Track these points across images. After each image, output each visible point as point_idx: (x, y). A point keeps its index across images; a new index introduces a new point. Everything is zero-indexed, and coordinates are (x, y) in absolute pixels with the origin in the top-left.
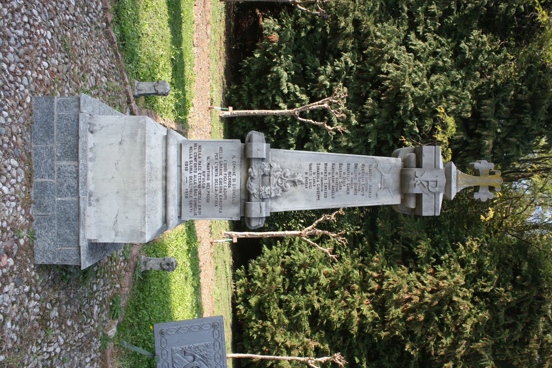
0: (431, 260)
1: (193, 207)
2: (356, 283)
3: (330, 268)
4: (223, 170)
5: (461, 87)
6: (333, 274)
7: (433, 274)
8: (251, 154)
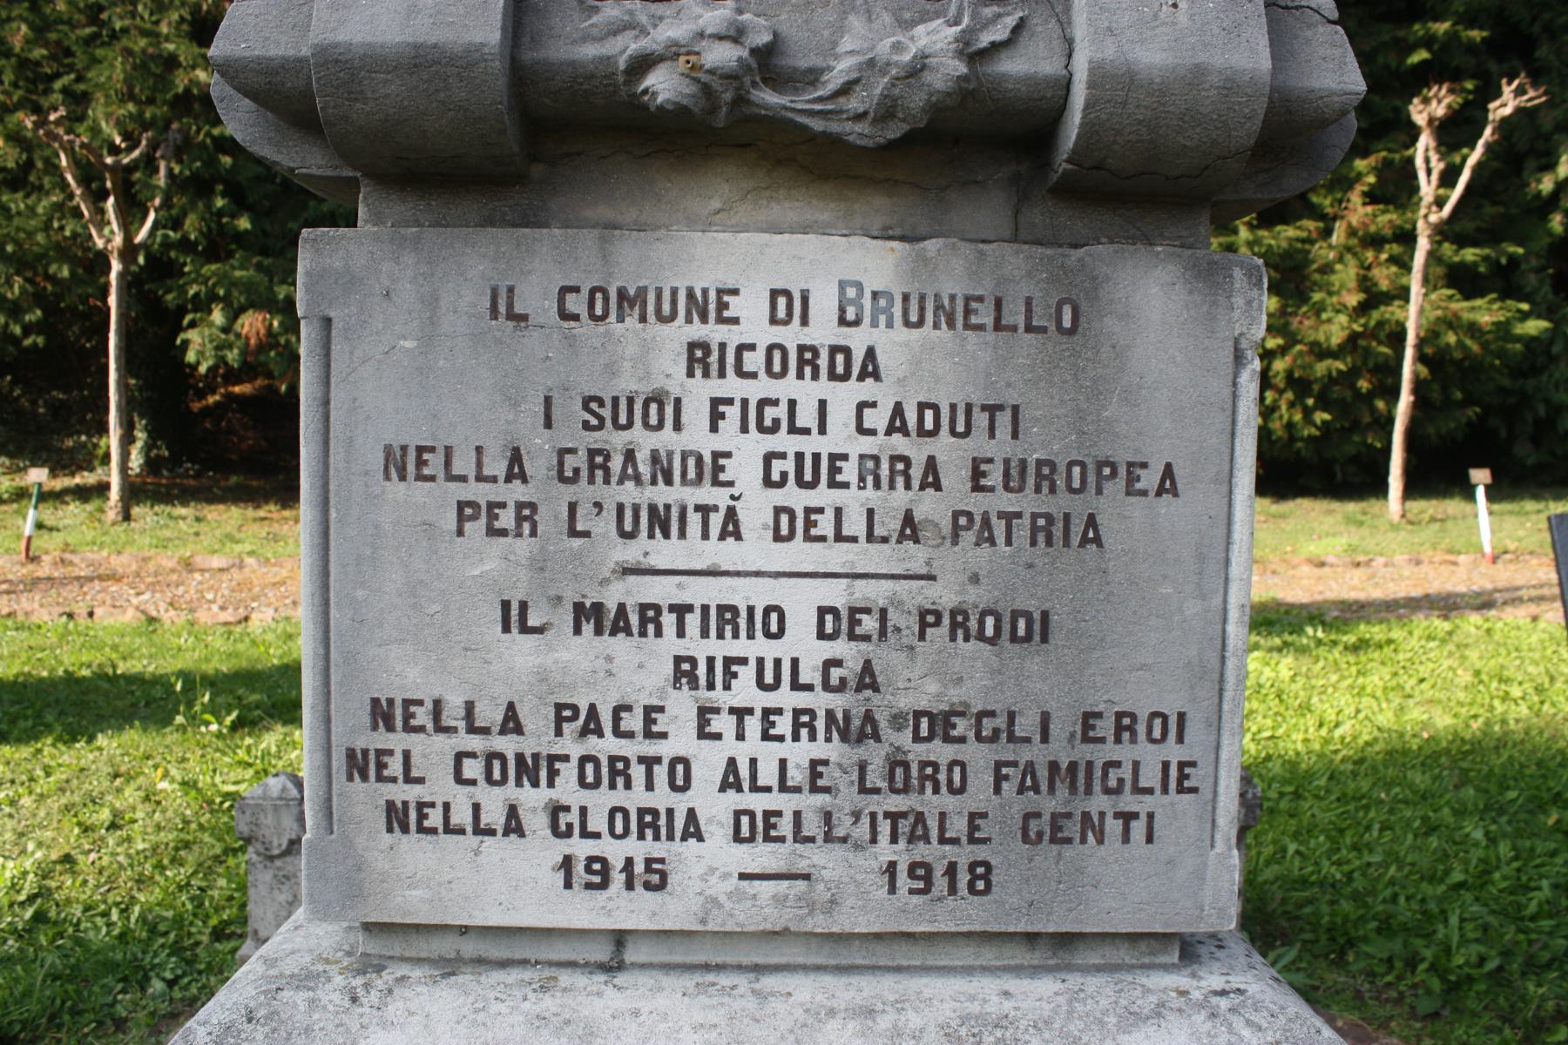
1: (1099, 803)
4: (666, 439)
8: (464, 62)
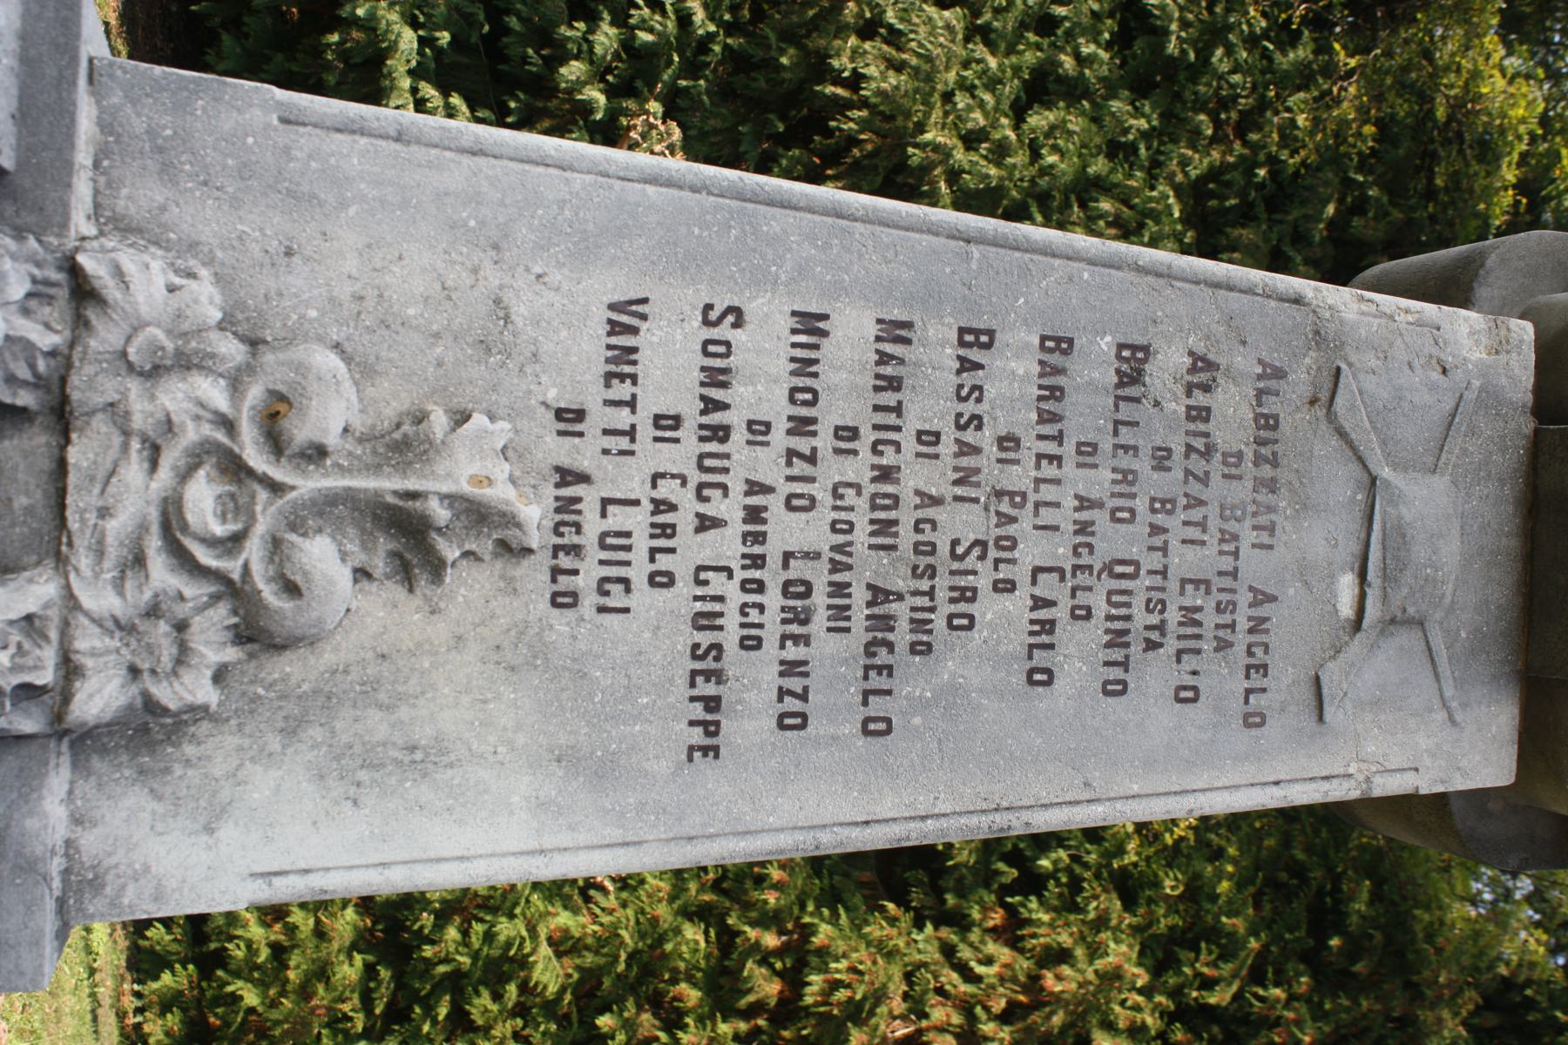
0: (997, 873)
2: (690, 979)
3: (576, 911)
5: (1141, 168)
6: (589, 941)
7: (1012, 932)
